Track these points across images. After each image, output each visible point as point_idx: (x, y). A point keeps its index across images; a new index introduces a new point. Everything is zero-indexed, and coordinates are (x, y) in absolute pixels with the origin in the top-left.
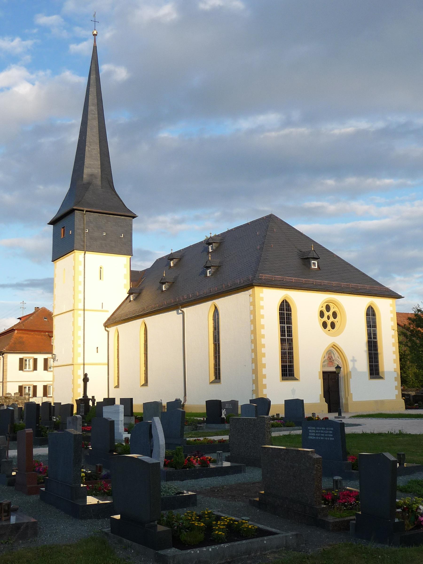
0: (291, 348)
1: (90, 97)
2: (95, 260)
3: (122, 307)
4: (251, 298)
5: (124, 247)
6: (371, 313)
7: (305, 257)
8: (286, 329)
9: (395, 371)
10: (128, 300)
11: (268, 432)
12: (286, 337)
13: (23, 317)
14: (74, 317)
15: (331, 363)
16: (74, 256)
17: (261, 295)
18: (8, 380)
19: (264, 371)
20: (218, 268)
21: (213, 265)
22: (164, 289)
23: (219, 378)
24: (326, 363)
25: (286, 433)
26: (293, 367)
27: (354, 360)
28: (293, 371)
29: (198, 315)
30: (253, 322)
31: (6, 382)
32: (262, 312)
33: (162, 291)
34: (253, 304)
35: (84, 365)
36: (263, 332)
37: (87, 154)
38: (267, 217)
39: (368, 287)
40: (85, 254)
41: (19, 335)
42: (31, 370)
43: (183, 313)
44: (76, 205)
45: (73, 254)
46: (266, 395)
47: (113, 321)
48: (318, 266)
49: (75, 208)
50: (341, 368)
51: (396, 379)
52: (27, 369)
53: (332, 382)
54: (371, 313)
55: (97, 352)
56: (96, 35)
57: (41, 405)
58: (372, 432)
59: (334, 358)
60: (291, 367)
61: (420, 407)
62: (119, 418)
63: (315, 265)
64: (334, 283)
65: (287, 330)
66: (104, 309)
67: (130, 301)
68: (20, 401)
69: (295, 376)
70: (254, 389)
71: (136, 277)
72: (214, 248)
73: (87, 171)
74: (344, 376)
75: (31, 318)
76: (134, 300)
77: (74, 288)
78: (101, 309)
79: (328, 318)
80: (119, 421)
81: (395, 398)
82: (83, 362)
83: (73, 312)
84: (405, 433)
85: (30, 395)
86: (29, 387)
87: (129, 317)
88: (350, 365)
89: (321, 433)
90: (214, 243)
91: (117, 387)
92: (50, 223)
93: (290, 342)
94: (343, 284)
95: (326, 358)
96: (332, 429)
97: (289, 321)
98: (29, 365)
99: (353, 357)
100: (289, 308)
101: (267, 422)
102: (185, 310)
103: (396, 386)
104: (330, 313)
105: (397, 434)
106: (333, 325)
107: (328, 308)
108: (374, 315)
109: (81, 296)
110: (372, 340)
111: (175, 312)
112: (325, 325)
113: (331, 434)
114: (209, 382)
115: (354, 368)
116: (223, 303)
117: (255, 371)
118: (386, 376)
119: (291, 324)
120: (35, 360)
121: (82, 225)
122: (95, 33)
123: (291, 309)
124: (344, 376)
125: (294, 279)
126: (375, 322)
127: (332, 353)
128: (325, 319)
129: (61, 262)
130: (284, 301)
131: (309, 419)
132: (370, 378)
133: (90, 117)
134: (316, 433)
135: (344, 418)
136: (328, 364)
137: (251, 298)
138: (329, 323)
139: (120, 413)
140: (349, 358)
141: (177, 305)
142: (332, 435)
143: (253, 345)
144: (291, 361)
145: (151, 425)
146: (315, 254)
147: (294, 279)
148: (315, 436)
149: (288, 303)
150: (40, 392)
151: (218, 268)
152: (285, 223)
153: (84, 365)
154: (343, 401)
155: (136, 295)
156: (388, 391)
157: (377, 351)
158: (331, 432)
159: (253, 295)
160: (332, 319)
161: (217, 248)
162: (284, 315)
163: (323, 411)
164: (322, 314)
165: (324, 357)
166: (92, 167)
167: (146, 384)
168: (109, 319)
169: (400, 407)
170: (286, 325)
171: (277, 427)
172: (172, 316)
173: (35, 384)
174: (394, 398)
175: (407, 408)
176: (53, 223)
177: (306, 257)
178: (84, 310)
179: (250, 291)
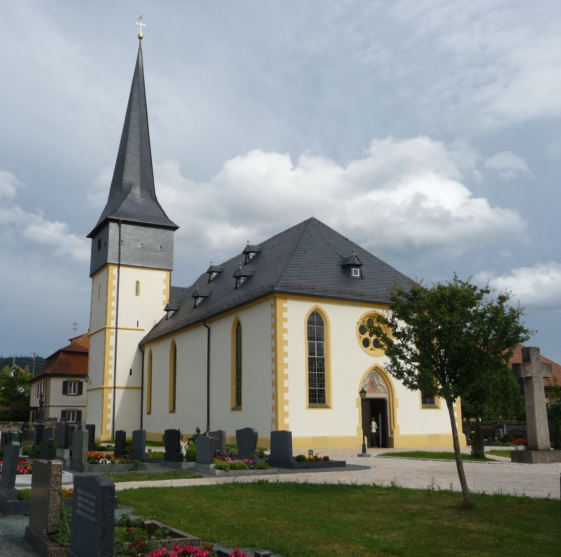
8: (316, 347)
11: (55, 491)
12: (316, 356)
15: (373, 389)
21: (242, 274)
25: (229, 480)
26: (324, 393)
34: (274, 316)
40: (119, 268)
44: (111, 214)
46: (287, 425)
48: (361, 274)
50: (366, 392)
58: (354, 483)
59: (377, 382)
60: (322, 392)
61: (489, 443)
82: (141, 386)
92: (89, 236)
95: (367, 382)
105: (388, 489)
112: (366, 343)
131: (300, 458)
132: (423, 408)
135: (369, 456)
136: (370, 389)
146: (356, 260)
159: (274, 306)
165: (364, 381)
171: (239, 469)
172: (200, 334)
173: (80, 409)
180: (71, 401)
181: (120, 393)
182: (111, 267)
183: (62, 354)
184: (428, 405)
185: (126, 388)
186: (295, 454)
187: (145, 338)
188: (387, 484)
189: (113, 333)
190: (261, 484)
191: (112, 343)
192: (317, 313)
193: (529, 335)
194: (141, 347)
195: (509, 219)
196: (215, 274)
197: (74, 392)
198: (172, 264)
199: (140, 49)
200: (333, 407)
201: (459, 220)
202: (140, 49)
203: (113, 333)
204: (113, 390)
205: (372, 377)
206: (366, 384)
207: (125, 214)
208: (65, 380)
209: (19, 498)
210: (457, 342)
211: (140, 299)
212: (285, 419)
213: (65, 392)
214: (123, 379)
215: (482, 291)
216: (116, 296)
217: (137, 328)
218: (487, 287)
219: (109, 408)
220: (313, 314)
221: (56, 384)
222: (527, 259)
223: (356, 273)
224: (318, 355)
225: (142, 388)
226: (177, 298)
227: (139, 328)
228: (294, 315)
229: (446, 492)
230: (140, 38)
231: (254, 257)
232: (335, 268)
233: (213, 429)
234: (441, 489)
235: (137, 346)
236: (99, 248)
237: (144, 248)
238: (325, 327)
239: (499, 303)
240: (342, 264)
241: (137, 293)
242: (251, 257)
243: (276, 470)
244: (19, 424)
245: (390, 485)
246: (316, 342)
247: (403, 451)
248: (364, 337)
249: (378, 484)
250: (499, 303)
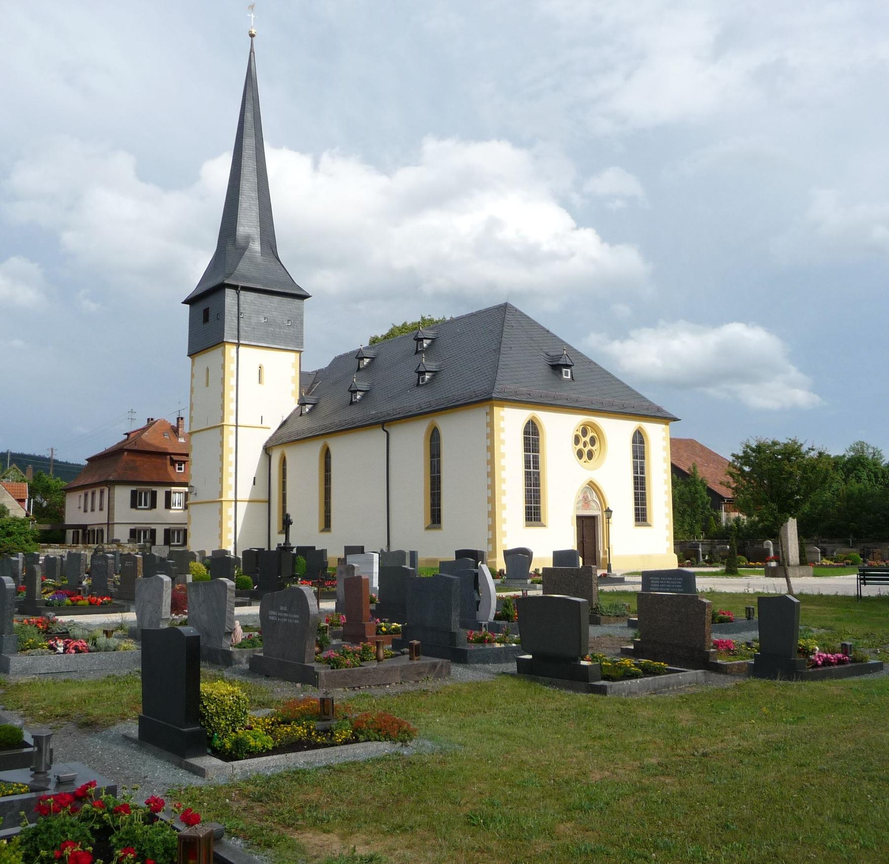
5: (289, 338)
6: (639, 439)
12: (532, 470)
23: (439, 522)
24: (580, 505)
34: (491, 425)
40: (238, 349)
48: (572, 376)
49: (226, 282)
52: (143, 507)
54: (639, 439)
60: (538, 509)
75: (146, 433)
78: (259, 424)
79: (585, 444)
92: (185, 302)
95: (581, 498)
97: (536, 450)
104: (587, 439)
106: (590, 455)
108: (642, 442)
112: (580, 454)
126: (643, 452)
128: (581, 446)
138: (586, 450)
145: (477, 575)
150: (160, 538)
159: (491, 414)
160: (589, 447)
164: (577, 440)
172: (377, 438)
173: (153, 527)
176: (191, 301)
180: (143, 517)
181: (242, 507)
182: (227, 347)
183: (126, 453)
184: (641, 523)
185: (249, 501)
187: (271, 439)
194: (267, 450)
195: (627, 260)
196: (367, 361)
197: (145, 505)
198: (302, 344)
199: (252, 51)
201: (553, 256)
202: (252, 51)
204: (233, 503)
205: (585, 492)
207: (245, 278)
208: (134, 488)
211: (262, 387)
213: (134, 505)
214: (245, 491)
216: (235, 384)
217: (260, 425)
220: (528, 423)
221: (123, 494)
222: (649, 317)
223: (567, 374)
225: (269, 502)
227: (263, 425)
228: (510, 422)
230: (252, 36)
231: (429, 345)
232: (542, 368)
233: (393, 549)
235: (261, 448)
236: (206, 319)
237: (268, 323)
238: (541, 437)
241: (260, 381)
242: (425, 345)
244: (90, 548)
246: (532, 454)
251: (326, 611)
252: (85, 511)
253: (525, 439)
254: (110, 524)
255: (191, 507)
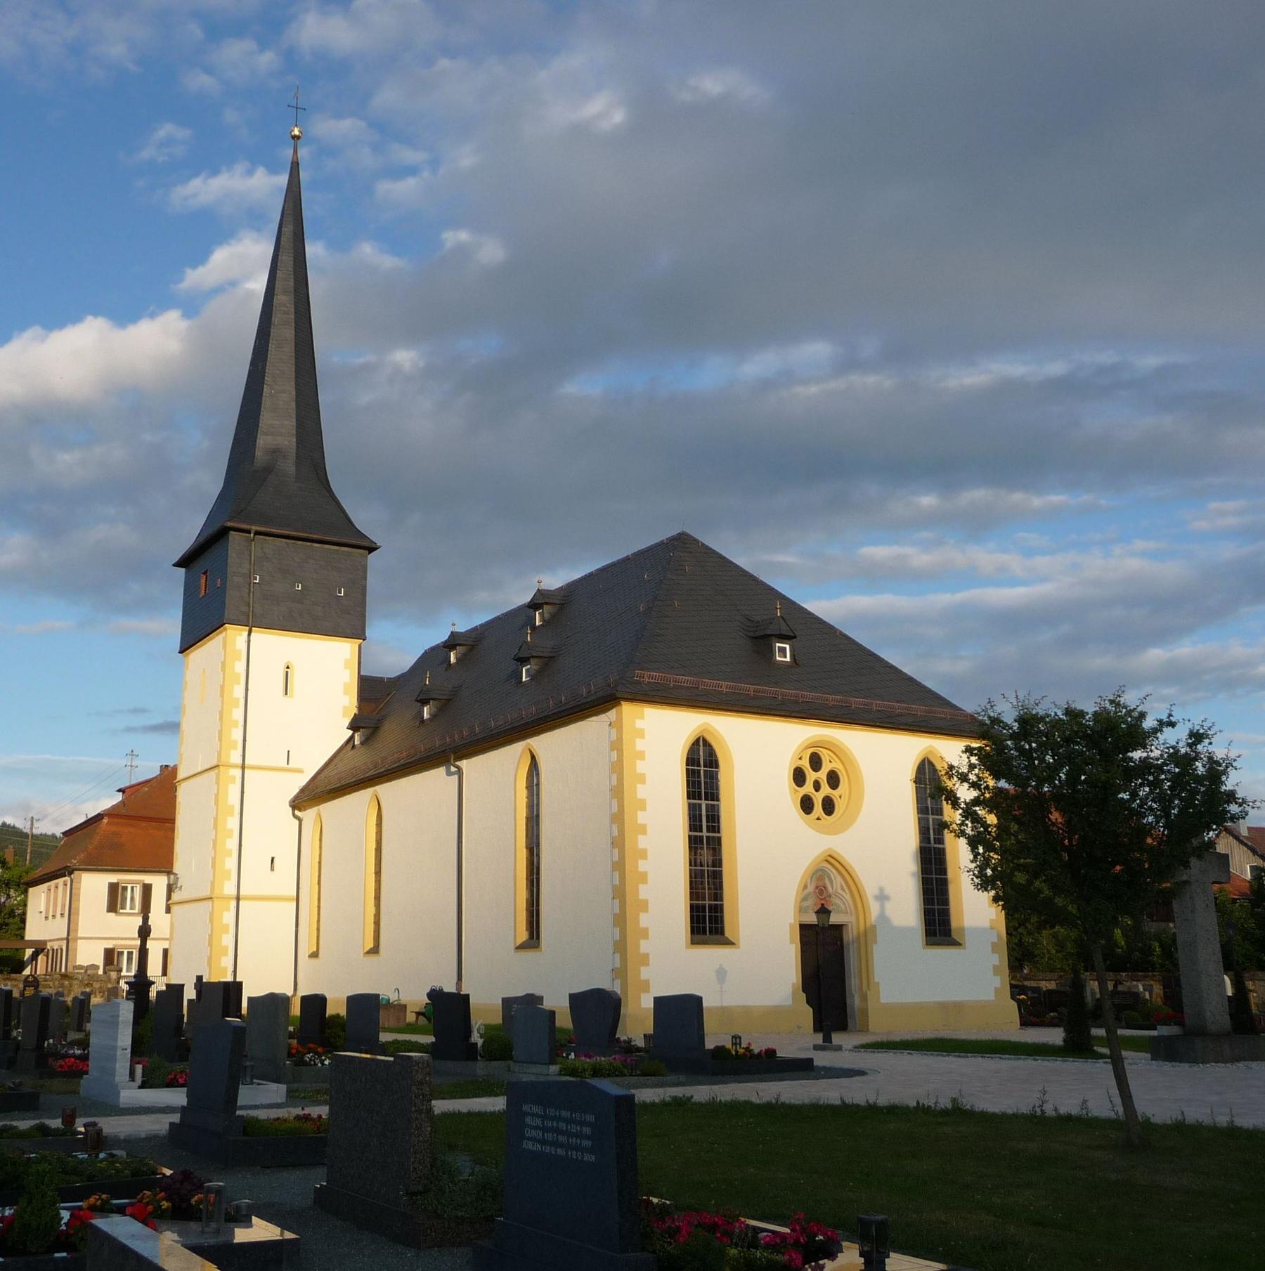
0: (718, 862)
1: (279, 274)
2: (273, 648)
3: (335, 761)
4: (614, 731)
5: (342, 618)
7: (758, 634)
8: (704, 812)
9: (992, 928)
10: (350, 745)
11: (421, 1112)
13: (130, 787)
14: (217, 783)
16: (225, 639)
17: (639, 724)
18: (80, 935)
19: (644, 920)
20: (548, 661)
22: (426, 716)
26: (722, 911)
27: (882, 897)
28: (722, 922)
29: (494, 774)
30: (617, 791)
31: (77, 939)
32: (641, 767)
33: (423, 721)
34: (617, 746)
35: (238, 899)
36: (642, 818)
37: (266, 402)
38: (673, 539)
39: (919, 709)
40: (249, 635)
41: (114, 829)
42: (136, 911)
43: (460, 772)
45: (221, 636)
47: (317, 793)
48: (793, 656)
49: (229, 524)
51: (995, 947)
52: (128, 910)
53: (826, 954)
55: (272, 869)
56: (298, 137)
57: (190, 994)
62: (116, 1040)
63: (783, 653)
64: (832, 699)
65: (707, 816)
66: (291, 765)
67: (354, 746)
68: (96, 985)
69: (727, 934)
70: (618, 965)
71: (374, 694)
72: (547, 616)
73: (262, 441)
74: (858, 938)
76: (362, 743)
77: (221, 713)
79: (817, 786)
80: (114, 1048)
81: (993, 998)
83: (216, 771)
84: (968, 1107)
85: (121, 970)
86: (130, 954)
87: (343, 783)
88: (874, 909)
89: (559, 1131)
90: (547, 604)
91: (315, 955)
92: (179, 564)
93: (715, 845)
94: (856, 702)
95: (811, 888)
96: (590, 1118)
97: (713, 795)
98: (132, 899)
99: (881, 889)
100: (712, 762)
101: (420, 1077)
102: (464, 764)
103: (994, 966)
104: (822, 775)
105: (945, 1112)
106: (829, 807)
107: (816, 762)
109: (237, 734)
110: (933, 845)
111: (442, 770)
112: (806, 805)
113: (588, 1138)
114: (513, 948)
115: (883, 916)
116: (548, 745)
117: (620, 920)
118: (968, 940)
119: (718, 800)
120: (147, 889)
121: (247, 565)
122: (296, 132)
123: (717, 761)
124: (858, 938)
125: (725, 686)
127: (826, 881)
128: (808, 788)
129: (199, 655)
130: (698, 740)
131: (720, 1051)
133: (276, 319)
134: (544, 1129)
135: (839, 1048)
137: (614, 731)
138: (818, 798)
139: (121, 1026)
140: (870, 890)
141: (444, 752)
142: (588, 1143)
143: (616, 851)
144: (717, 893)
147: (725, 686)
148: (543, 1142)
149: (710, 746)
151: (548, 661)
152: (714, 552)
153: (238, 899)
154: (855, 1001)
155: (367, 732)
156: (971, 976)
157: (945, 873)
158: (587, 1130)
159: (617, 725)
160: (826, 790)
161: (554, 616)
162: (699, 776)
163: (799, 1027)
164: (799, 777)
165: (805, 887)
166: (277, 430)
167: (375, 950)
168: (302, 791)
169: (1005, 1021)
170: (704, 803)
172: (436, 780)
174: (991, 996)
175: (1024, 1023)
177: (761, 633)
178: (243, 767)
179: (612, 714)
186: (710, 1044)
188: (945, 1103)
189: (234, 778)
190: (679, 1103)
191: (234, 799)
192: (705, 741)
193: (1248, 809)
200: (967, 944)
203: (234, 778)
204: (233, 903)
206: (809, 894)
209: (245, 1133)
210: (1079, 820)
212: (642, 969)
215: (1161, 722)
218: (1170, 715)
219: (224, 943)
220: (696, 743)
224: (708, 831)
226: (375, 698)
229: (1069, 1118)
234: (1062, 1112)
239: (1190, 745)
240: (752, 634)
243: (682, 1078)
245: (949, 1106)
247: (908, 1037)
248: (802, 791)
249: (930, 1102)
250: (1190, 745)
251: (1100, 1026)
252: (46, 918)
253: (690, 774)
254: (70, 938)
255: (174, 909)
